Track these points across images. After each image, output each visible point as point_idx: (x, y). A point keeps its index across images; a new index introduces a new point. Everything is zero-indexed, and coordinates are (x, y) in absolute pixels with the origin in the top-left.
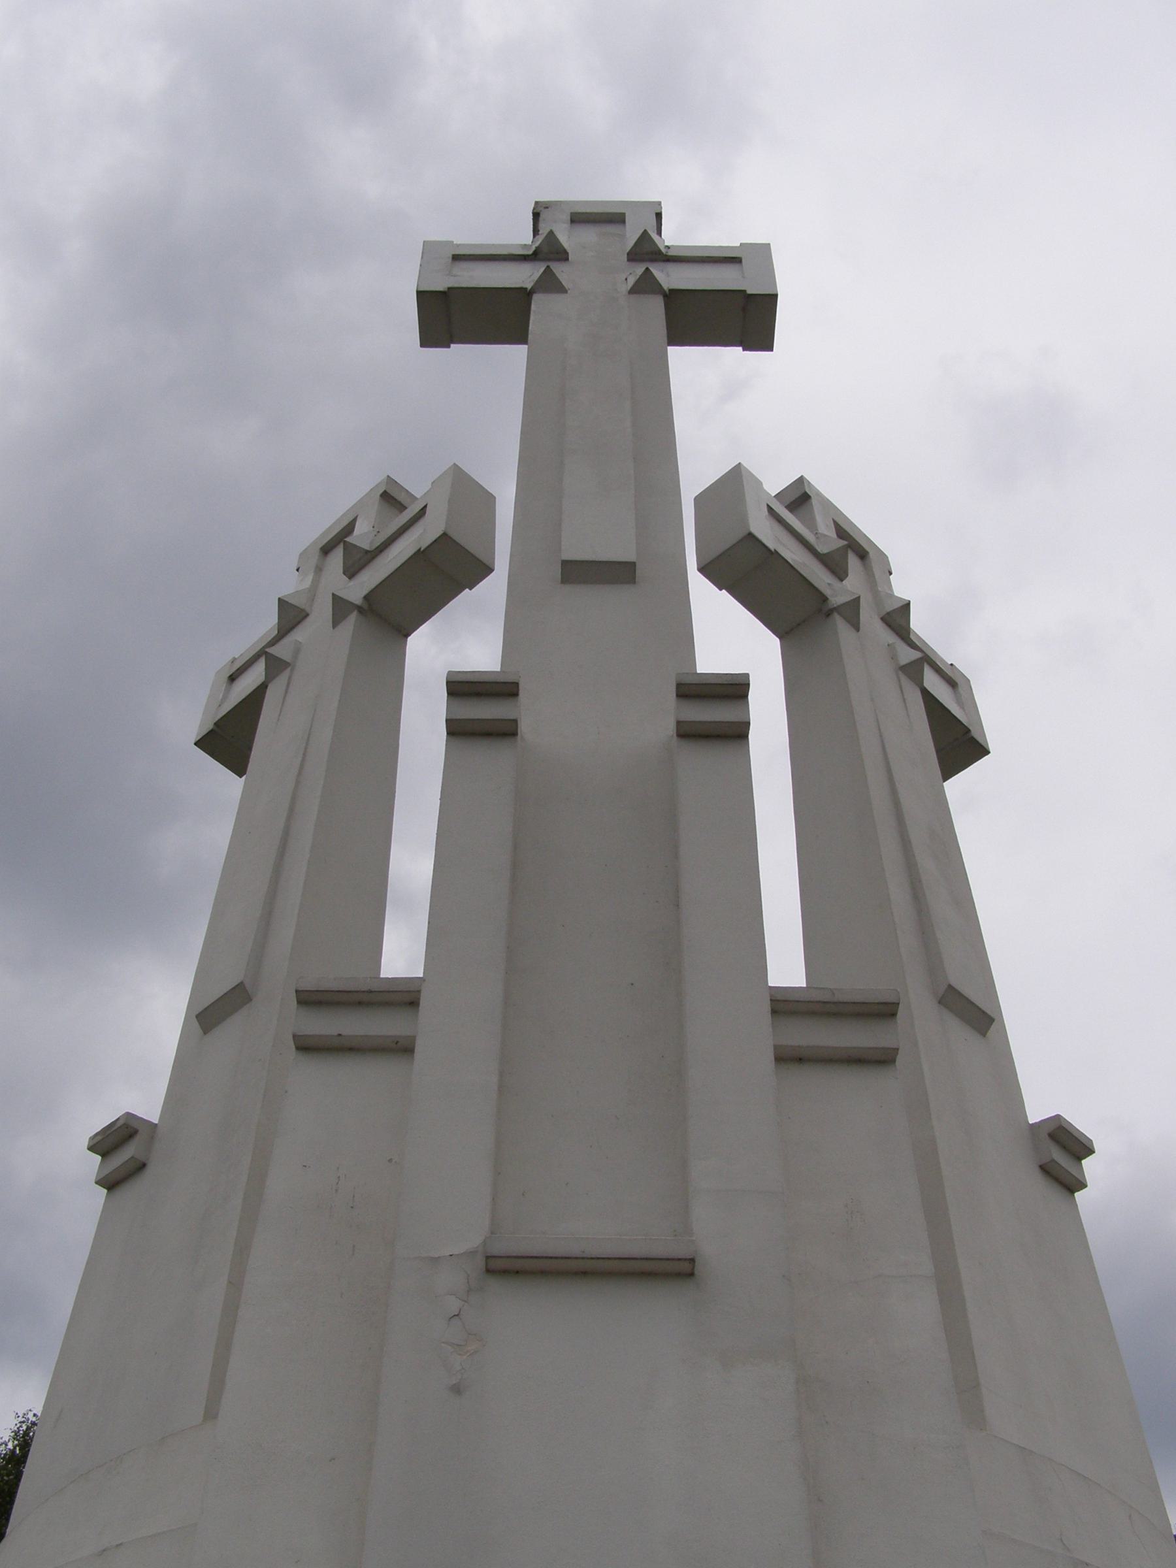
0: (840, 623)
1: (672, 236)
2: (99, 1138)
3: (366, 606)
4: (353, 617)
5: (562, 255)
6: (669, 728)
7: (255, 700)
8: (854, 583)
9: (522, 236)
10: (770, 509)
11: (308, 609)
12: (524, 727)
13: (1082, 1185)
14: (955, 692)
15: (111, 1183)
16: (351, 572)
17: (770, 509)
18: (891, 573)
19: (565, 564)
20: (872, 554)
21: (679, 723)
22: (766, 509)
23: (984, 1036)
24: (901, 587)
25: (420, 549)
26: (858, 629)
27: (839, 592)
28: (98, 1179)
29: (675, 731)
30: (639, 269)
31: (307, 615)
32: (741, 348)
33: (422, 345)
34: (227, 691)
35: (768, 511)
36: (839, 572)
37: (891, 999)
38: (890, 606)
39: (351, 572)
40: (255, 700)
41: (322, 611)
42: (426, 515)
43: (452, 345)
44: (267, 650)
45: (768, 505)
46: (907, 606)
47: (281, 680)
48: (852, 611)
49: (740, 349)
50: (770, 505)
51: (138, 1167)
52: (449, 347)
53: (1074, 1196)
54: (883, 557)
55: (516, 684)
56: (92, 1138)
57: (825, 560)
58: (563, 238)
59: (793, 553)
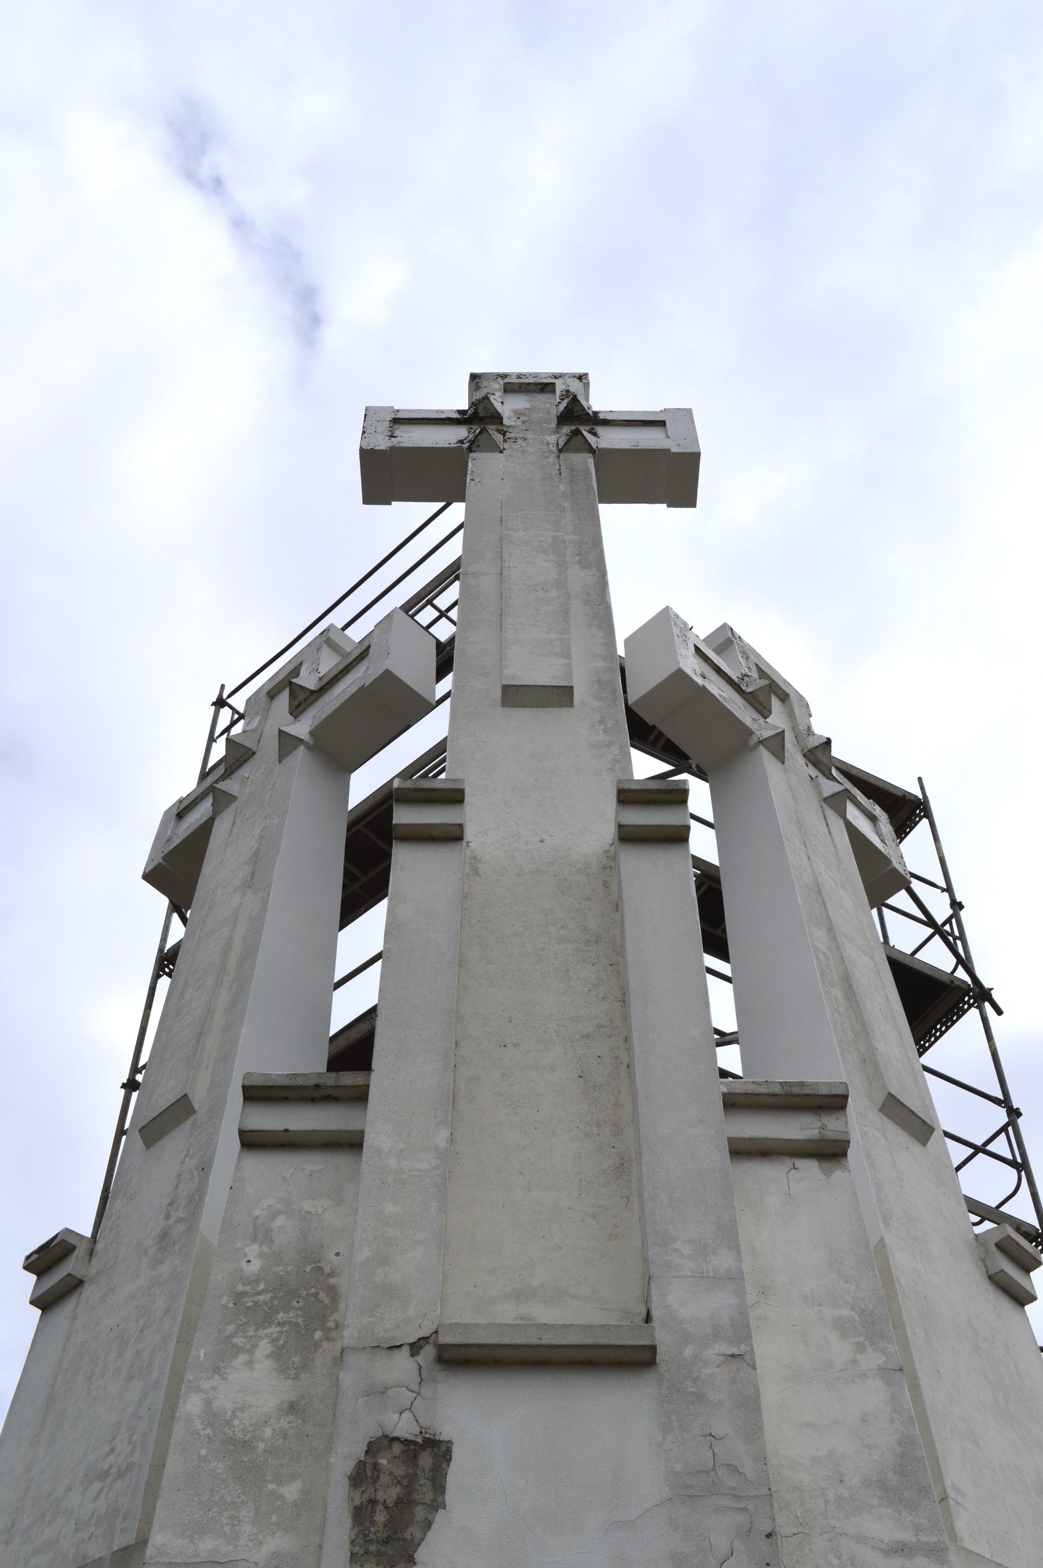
0: (765, 756)
1: (599, 401)
2: (35, 1256)
3: (311, 742)
4: (301, 751)
5: (497, 418)
6: (609, 832)
7: (204, 831)
8: (778, 719)
9: (459, 401)
10: (697, 649)
11: (254, 749)
12: (469, 833)
13: (1033, 1298)
14: (875, 826)
15: (45, 1302)
16: (297, 710)
17: (697, 649)
18: (810, 716)
19: (506, 689)
20: (792, 696)
21: (620, 826)
22: (693, 648)
23: (925, 1146)
24: (821, 726)
25: (364, 685)
26: (783, 763)
27: (762, 729)
28: (31, 1300)
29: (617, 834)
30: (566, 429)
31: (254, 753)
32: (665, 505)
33: (364, 503)
34: (176, 827)
35: (696, 651)
36: (764, 711)
37: (839, 1091)
38: (812, 743)
39: (297, 710)
40: (204, 831)
41: (271, 745)
42: (370, 655)
43: (393, 502)
44: (215, 785)
45: (695, 646)
46: (829, 742)
47: (229, 813)
48: (776, 745)
49: (665, 505)
50: (696, 644)
51: (73, 1285)
52: (390, 504)
53: (1024, 1310)
54: (801, 698)
55: (461, 792)
56: (28, 1258)
57: (751, 699)
58: (496, 401)
59: (717, 688)
